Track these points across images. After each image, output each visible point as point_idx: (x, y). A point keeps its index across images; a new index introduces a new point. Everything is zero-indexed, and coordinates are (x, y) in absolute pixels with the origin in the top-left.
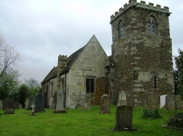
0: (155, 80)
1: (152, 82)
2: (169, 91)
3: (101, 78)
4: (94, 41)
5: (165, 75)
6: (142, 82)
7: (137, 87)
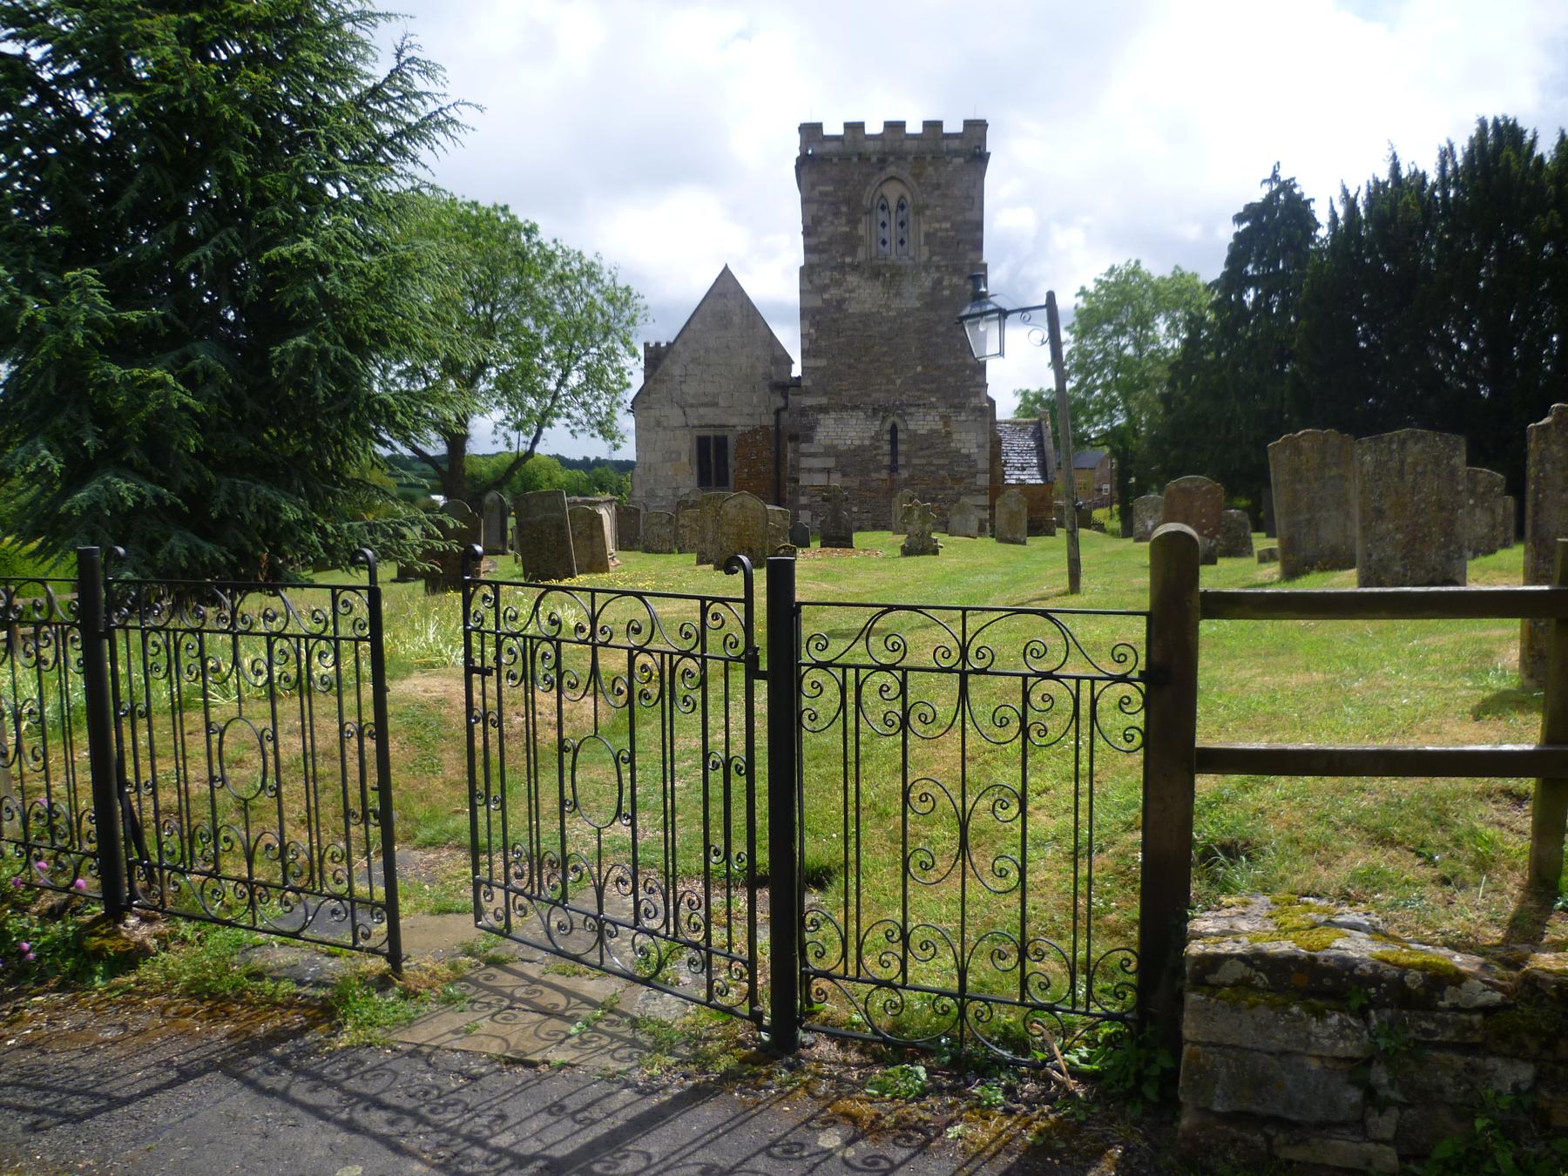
0: (894, 442)
1: (877, 448)
2: (962, 479)
3: (755, 431)
4: (726, 288)
5: (942, 417)
6: (831, 451)
7: (810, 470)
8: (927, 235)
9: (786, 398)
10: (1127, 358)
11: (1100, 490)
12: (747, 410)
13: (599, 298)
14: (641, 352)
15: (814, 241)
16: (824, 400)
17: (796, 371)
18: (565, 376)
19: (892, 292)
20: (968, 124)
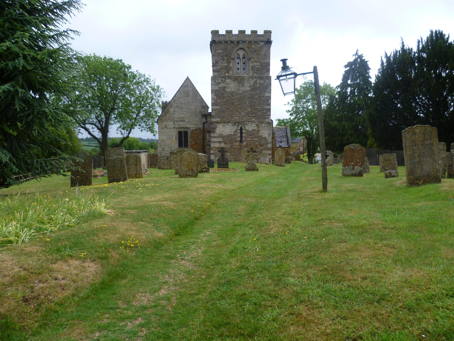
0: (241, 133)
1: (236, 135)
3: (197, 129)
4: (188, 89)
5: (257, 125)
6: (221, 136)
7: (214, 142)
8: (252, 67)
9: (206, 119)
10: (310, 110)
11: (299, 149)
12: (194, 123)
13: (150, 89)
14: (161, 104)
15: (216, 68)
16: (219, 120)
17: (210, 110)
18: (139, 113)
19: (241, 85)
20: (265, 32)
